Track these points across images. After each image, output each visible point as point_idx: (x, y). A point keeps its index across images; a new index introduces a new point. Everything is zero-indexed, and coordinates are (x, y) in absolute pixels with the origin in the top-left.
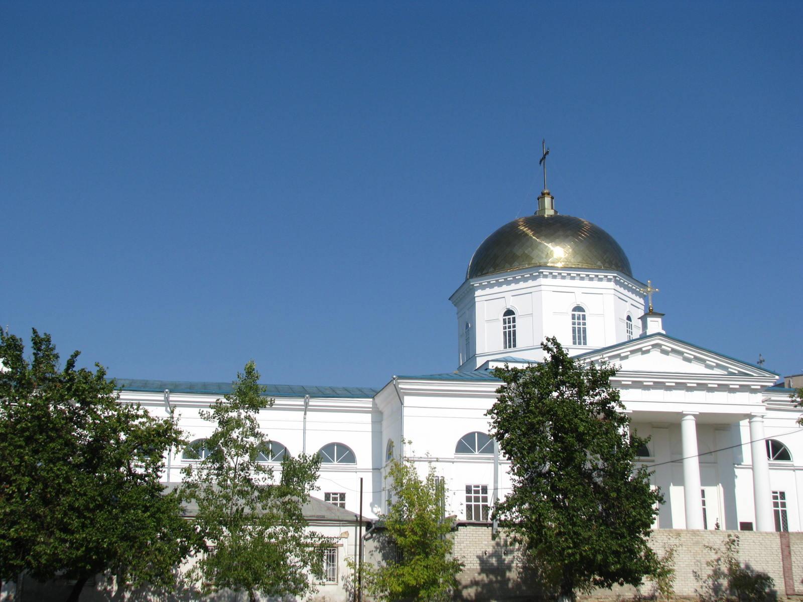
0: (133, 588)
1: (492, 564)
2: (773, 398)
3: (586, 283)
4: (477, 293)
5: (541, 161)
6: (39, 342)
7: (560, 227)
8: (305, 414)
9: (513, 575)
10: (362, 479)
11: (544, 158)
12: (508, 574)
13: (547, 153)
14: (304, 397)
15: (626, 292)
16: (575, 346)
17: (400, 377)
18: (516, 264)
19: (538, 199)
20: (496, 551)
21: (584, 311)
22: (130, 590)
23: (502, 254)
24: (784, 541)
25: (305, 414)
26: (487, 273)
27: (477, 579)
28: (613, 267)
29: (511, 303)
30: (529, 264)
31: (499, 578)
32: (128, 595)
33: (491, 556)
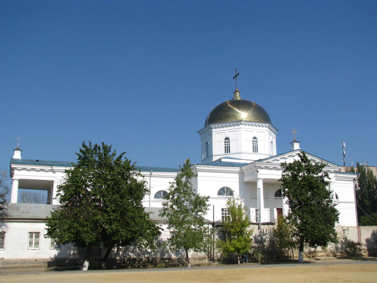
0: (123, 250)
1: (259, 240)
2: (338, 176)
3: (258, 128)
4: (213, 130)
5: (234, 78)
6: (105, 148)
7: (243, 104)
8: (150, 178)
9: (266, 244)
10: (214, 206)
11: (236, 76)
12: (264, 243)
13: (238, 74)
14: (150, 171)
15: (272, 133)
16: (254, 153)
17: (197, 164)
18: (230, 119)
19: (234, 93)
20: (260, 234)
21: (229, 139)
22: (122, 251)
23: (220, 115)
24: (359, 230)
25: (150, 178)
26: (217, 122)
27: (253, 245)
28: (267, 121)
29: (228, 135)
30: (235, 119)
31: (261, 245)
32: (121, 253)
33: (258, 236)
